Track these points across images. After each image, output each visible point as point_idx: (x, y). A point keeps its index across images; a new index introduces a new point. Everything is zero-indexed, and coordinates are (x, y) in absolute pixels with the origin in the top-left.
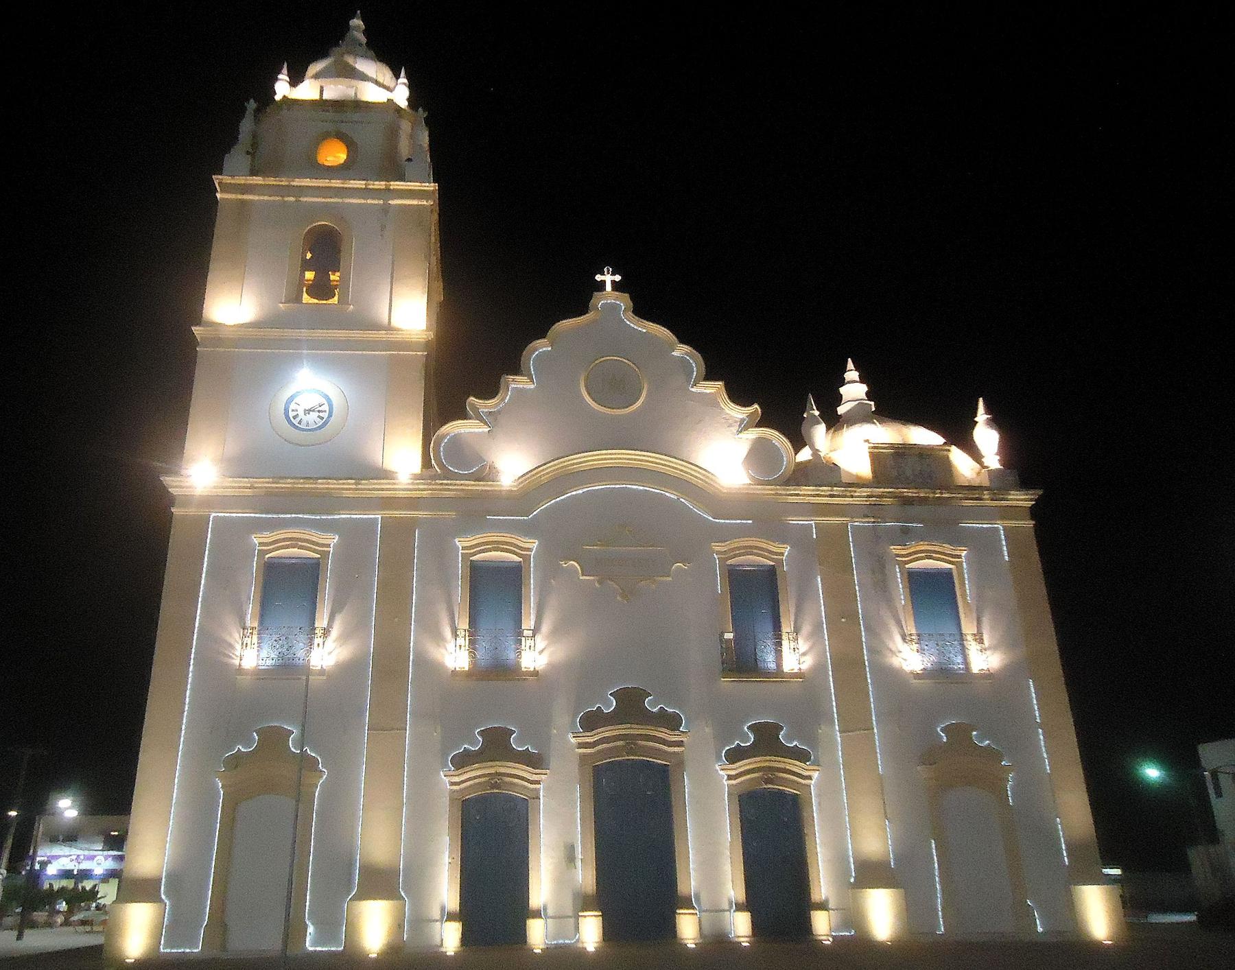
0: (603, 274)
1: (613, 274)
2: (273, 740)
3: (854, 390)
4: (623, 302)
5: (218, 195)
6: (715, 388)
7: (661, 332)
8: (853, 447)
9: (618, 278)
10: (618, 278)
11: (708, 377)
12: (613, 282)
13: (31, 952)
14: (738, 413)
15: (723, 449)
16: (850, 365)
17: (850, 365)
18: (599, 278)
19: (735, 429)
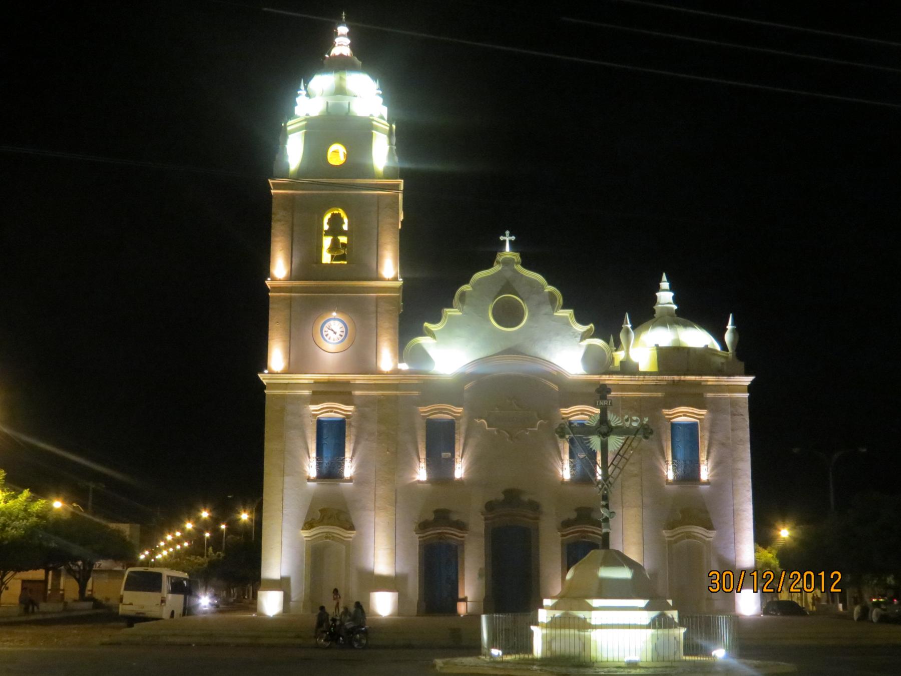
0: (505, 235)
1: (511, 235)
2: (651, 433)
3: (665, 297)
4: (516, 257)
5: (273, 191)
6: (568, 313)
7: (538, 277)
8: (644, 347)
9: (513, 238)
10: (513, 238)
11: (565, 307)
12: (510, 241)
13: (270, 447)
14: (581, 328)
15: (568, 352)
16: (664, 278)
17: (664, 278)
18: (502, 238)
19: (578, 339)
